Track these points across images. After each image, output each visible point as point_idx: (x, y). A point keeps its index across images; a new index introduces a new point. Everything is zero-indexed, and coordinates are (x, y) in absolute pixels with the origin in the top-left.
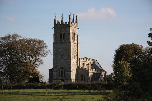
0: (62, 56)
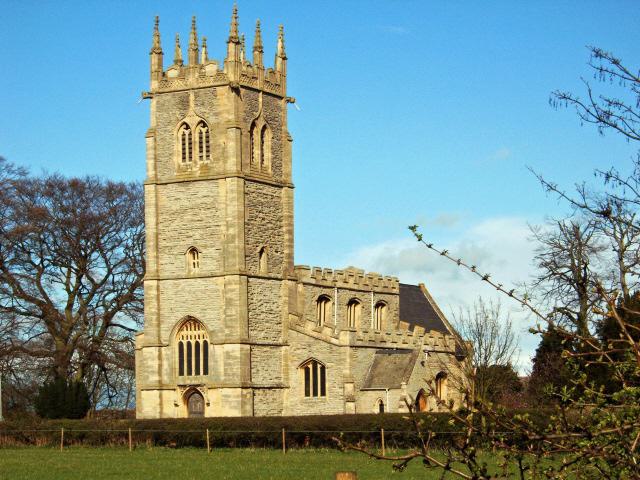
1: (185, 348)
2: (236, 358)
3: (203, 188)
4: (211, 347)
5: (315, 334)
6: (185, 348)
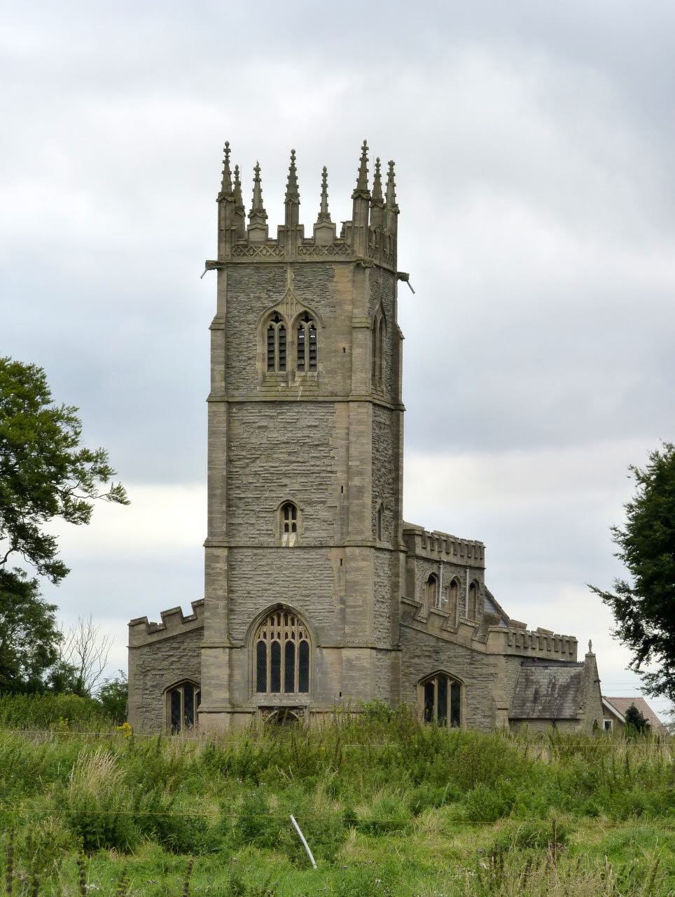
0: (288, 508)
1: (269, 651)
2: (362, 669)
3: (308, 417)
4: (314, 654)
5: (445, 636)
6: (269, 651)
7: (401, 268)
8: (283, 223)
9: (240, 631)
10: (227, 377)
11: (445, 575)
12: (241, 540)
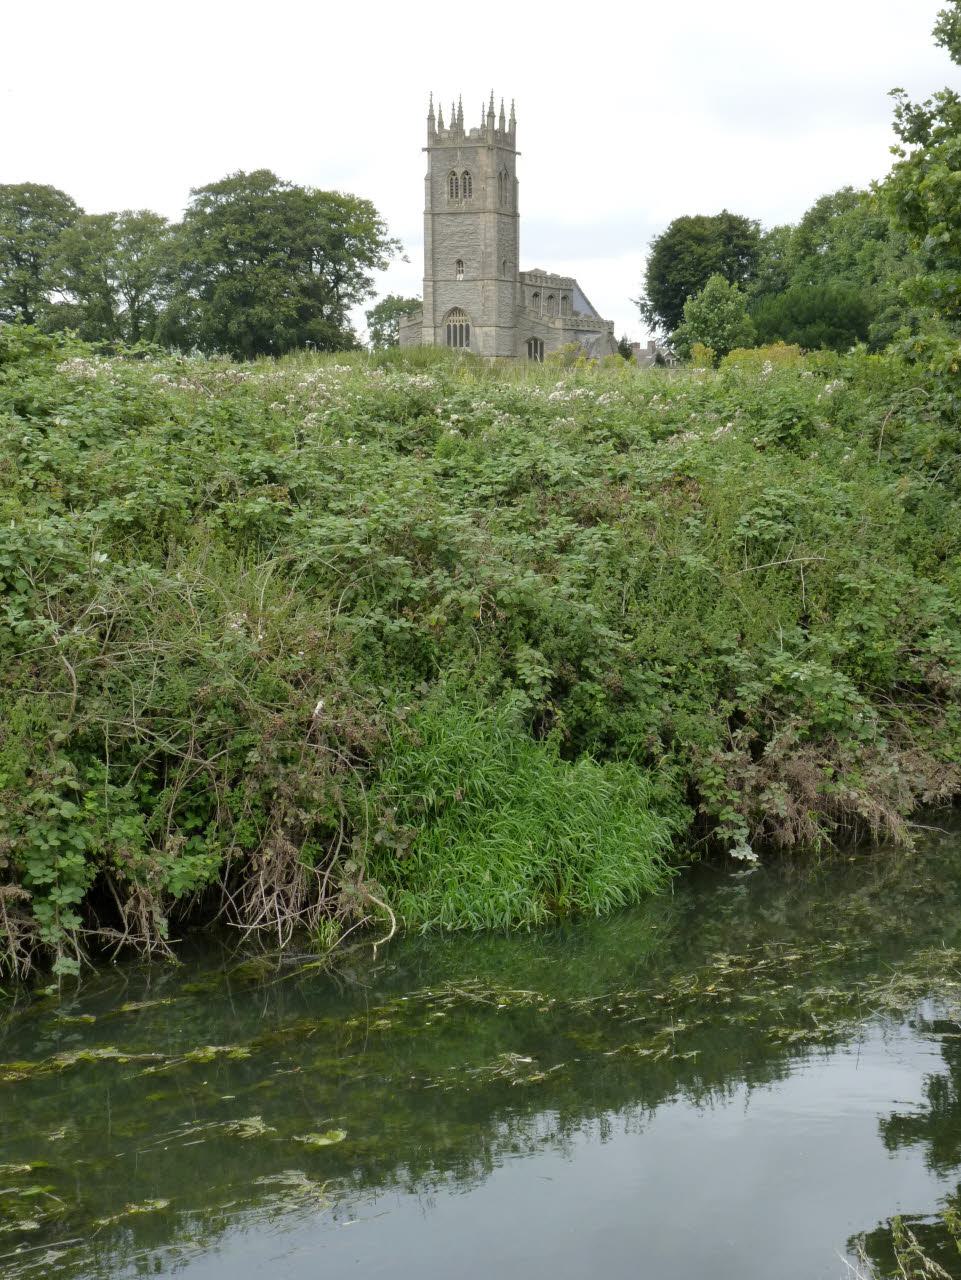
4: (471, 329)
7: (517, 150)
8: (247, 174)
9: (439, 319)
10: (432, 202)
11: (544, 293)
12: (439, 278)
